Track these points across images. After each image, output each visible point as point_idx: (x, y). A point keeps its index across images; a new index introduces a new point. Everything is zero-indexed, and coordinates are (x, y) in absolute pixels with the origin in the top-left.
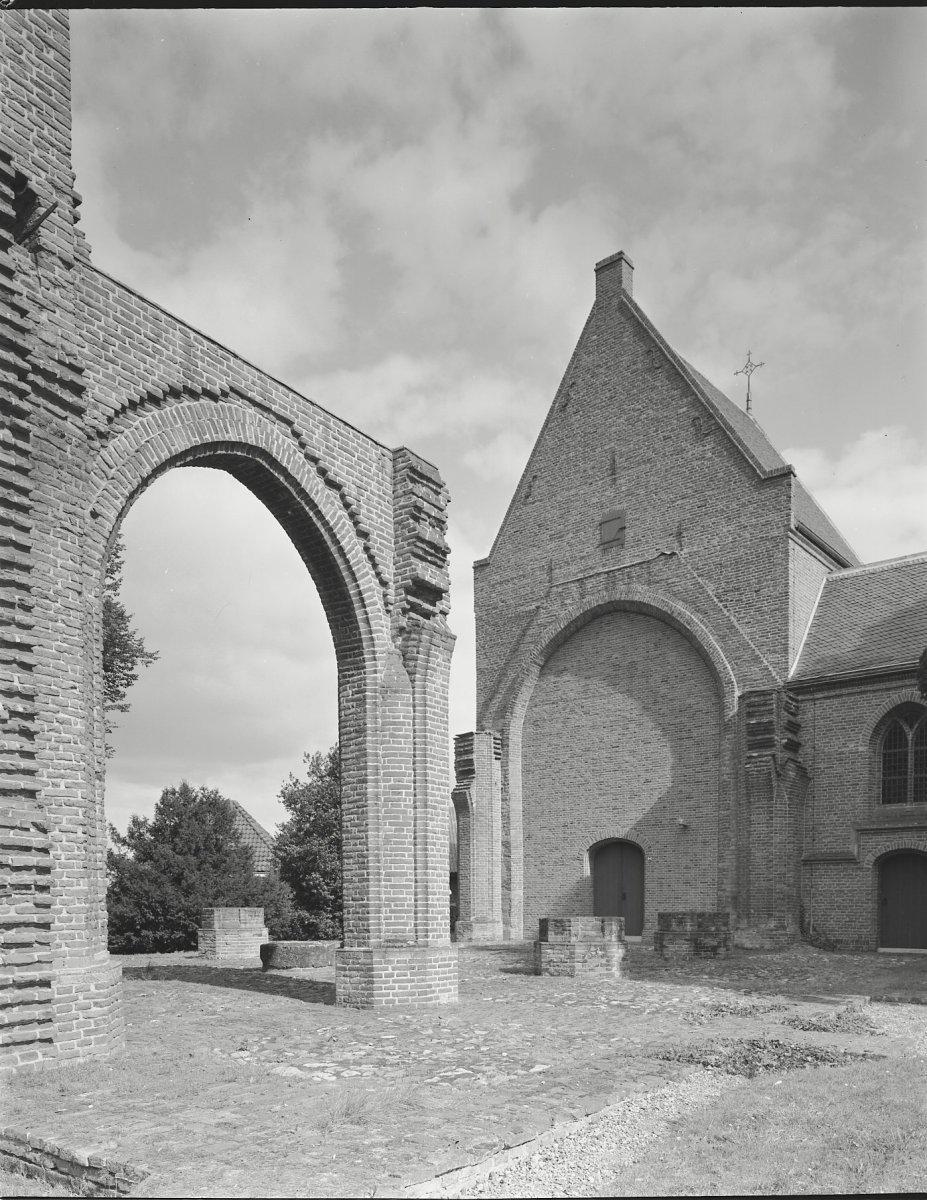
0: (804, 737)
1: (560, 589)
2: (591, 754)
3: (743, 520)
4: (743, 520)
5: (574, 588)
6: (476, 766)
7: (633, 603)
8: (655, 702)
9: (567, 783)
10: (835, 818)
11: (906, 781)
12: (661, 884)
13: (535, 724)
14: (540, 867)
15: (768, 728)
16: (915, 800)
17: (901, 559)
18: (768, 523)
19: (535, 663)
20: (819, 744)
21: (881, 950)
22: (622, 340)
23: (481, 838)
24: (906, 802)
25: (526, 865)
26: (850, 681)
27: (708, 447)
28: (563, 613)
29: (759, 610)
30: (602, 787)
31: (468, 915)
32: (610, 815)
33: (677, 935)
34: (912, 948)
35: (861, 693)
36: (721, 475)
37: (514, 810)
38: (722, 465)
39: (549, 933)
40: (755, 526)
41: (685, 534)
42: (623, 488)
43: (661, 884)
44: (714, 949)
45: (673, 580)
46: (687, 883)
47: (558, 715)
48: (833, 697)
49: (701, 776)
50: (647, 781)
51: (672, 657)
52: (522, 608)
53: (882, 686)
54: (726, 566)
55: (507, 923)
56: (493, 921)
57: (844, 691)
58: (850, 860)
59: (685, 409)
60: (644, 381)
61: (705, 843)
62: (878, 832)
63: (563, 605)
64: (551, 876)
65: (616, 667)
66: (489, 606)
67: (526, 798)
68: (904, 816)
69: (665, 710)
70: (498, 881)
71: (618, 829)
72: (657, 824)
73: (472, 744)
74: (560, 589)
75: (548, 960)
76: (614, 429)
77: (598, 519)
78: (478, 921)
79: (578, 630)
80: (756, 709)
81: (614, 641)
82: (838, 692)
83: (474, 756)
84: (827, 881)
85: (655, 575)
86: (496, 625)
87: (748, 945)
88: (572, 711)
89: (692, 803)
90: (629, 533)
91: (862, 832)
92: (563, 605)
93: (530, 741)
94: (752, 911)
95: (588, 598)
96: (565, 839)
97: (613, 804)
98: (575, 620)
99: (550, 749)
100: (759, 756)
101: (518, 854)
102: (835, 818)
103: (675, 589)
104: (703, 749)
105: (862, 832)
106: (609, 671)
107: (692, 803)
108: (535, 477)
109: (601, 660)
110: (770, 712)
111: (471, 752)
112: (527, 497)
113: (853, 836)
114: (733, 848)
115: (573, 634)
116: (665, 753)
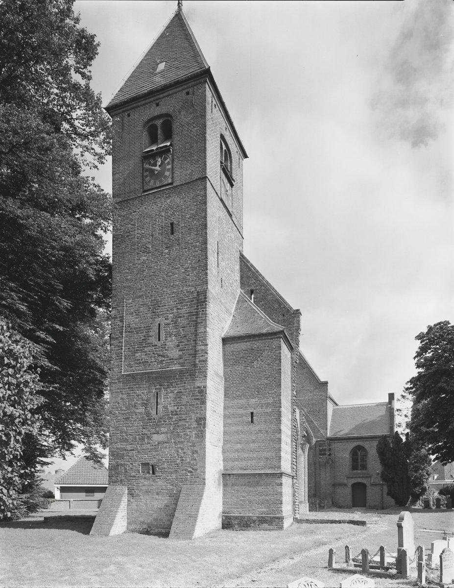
0: (332, 452)
4: (314, 393)
11: (358, 458)
15: (325, 450)
22: (178, 23)
24: (358, 470)
44: (324, 507)
57: (343, 441)
62: (352, 478)
68: (358, 474)
70: (308, 525)
84: (339, 490)
105: (348, 478)
110: (326, 446)
113: (346, 479)
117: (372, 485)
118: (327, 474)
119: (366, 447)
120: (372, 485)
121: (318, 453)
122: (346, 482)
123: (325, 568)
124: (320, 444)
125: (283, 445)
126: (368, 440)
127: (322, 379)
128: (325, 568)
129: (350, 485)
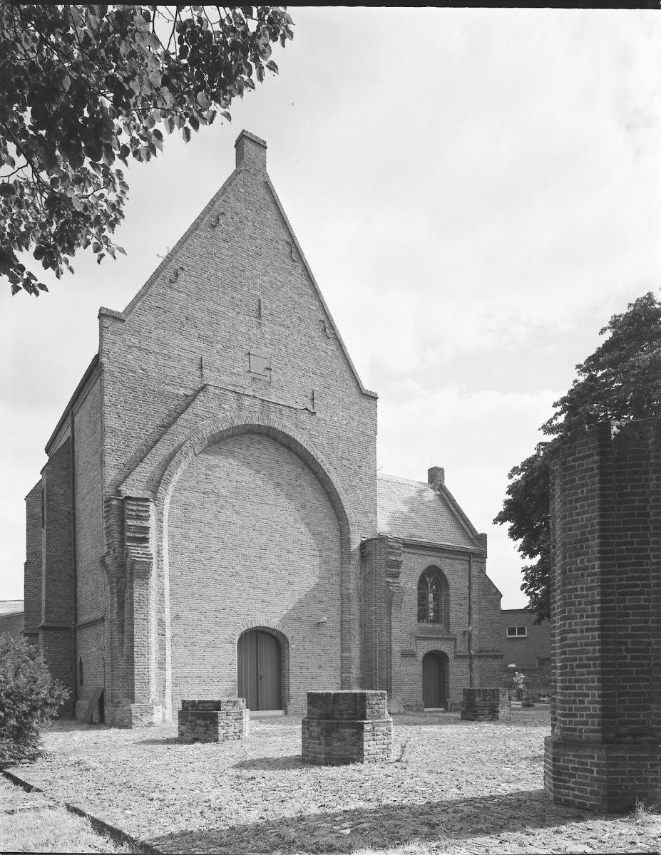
7: (287, 436)
9: (219, 571)
13: (185, 507)
14: (191, 648)
21: (425, 710)
28: (221, 416)
34: (438, 707)
36: (338, 373)
45: (314, 433)
46: (320, 667)
49: (328, 587)
51: (309, 491)
61: (332, 637)
62: (425, 639)
64: (203, 657)
66: (123, 364)
71: (270, 618)
74: (218, 392)
79: (232, 436)
88: (223, 507)
91: (418, 638)
95: (244, 413)
96: (217, 624)
98: (235, 428)
99: (201, 535)
100: (393, 583)
104: (330, 567)
113: (413, 640)
120: (457, 657)
127: (367, 385)
129: (420, 655)
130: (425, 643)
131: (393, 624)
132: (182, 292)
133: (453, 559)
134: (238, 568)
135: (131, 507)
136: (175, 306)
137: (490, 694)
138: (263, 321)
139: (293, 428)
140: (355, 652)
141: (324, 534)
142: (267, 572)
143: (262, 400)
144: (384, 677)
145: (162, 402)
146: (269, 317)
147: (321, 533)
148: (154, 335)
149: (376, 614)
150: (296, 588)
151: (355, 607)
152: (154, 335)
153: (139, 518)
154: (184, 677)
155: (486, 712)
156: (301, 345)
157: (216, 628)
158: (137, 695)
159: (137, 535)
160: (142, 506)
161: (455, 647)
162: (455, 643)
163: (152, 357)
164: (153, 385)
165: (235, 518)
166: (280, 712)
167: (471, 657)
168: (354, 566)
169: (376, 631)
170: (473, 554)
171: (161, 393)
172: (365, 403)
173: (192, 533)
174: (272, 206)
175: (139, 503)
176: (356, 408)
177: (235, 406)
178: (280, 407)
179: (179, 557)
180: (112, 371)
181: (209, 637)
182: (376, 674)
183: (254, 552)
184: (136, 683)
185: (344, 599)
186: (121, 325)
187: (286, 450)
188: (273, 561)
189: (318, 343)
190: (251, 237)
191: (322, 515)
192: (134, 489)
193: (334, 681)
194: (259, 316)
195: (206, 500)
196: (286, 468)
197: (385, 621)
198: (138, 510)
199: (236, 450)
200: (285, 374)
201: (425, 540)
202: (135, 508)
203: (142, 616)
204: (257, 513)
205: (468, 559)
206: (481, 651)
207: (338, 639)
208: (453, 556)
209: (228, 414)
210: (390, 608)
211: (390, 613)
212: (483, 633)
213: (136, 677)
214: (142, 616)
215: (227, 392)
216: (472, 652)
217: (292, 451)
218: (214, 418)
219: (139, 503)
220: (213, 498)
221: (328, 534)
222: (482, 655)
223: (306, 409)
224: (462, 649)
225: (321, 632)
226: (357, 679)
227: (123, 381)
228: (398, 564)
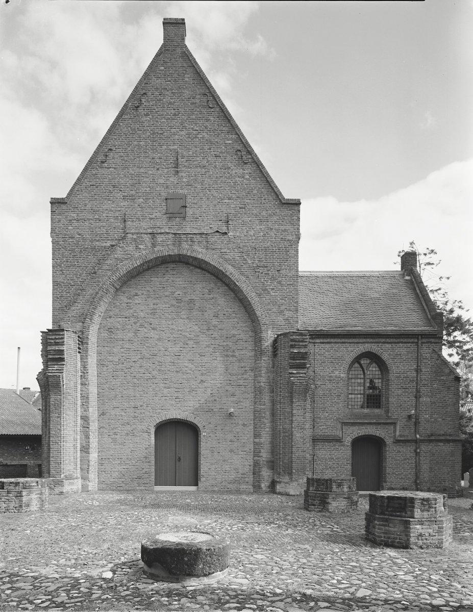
1: (135, 237)
2: (158, 358)
3: (270, 224)
4: (270, 224)
5: (147, 238)
6: (65, 356)
7: (195, 259)
8: (208, 329)
10: (327, 415)
12: (213, 452)
13: (110, 330)
14: (113, 436)
16: (368, 407)
17: (330, 272)
18: (285, 231)
19: (113, 286)
20: (317, 370)
23: (68, 412)
25: (101, 434)
26: (338, 335)
27: (246, 171)
28: (137, 255)
29: (280, 282)
30: (167, 382)
31: (59, 473)
32: (173, 402)
33: (338, 495)
35: (343, 343)
36: (255, 192)
37: (91, 393)
38: (256, 185)
39: (415, 510)
40: (277, 230)
41: (230, 223)
42: (184, 180)
43: (213, 452)
45: (225, 250)
46: (231, 451)
47: (129, 327)
48: (326, 343)
49: (241, 382)
50: (202, 381)
51: (222, 301)
52: (97, 243)
53: (354, 340)
54: (259, 250)
55: (84, 478)
56: (77, 478)
58: (339, 440)
59: (230, 142)
60: (201, 112)
61: (244, 425)
62: (353, 424)
63: (137, 247)
64: (123, 444)
65: (179, 300)
66: (65, 235)
67: (99, 385)
69: (216, 334)
72: (210, 411)
73: (63, 338)
74: (135, 237)
75: (416, 534)
76: (177, 137)
77: (164, 195)
78: (67, 478)
79: (149, 269)
80: (297, 343)
81: (179, 282)
82: (328, 340)
83: (65, 348)
85: (212, 244)
86: (73, 251)
87: (292, 493)
88: (142, 326)
89: (235, 399)
90: (190, 212)
92: (137, 247)
93: (100, 343)
94: (294, 471)
97: (176, 395)
99: (122, 350)
100: (297, 373)
101: (94, 426)
102: (327, 415)
103: (226, 257)
104: (243, 365)
106: (174, 302)
107: (235, 399)
108: (110, 150)
109: (167, 293)
111: (62, 344)
112: (103, 162)
113: (340, 426)
114: (268, 430)
115: (144, 271)
116: (218, 364)
117: (397, 442)
118: (307, 414)
119: (385, 357)
120: (397, 442)
121: (285, 363)
122: (339, 433)
123: (48, 587)
124: (292, 340)
125: (96, 391)
126: (388, 340)
127: (288, 194)
128: (48, 587)
129: (348, 440)
130: (355, 428)
131: (294, 412)
132: (111, 167)
133: (395, 343)
134: (154, 373)
135: (50, 337)
136: (105, 180)
137: (323, 484)
138: (181, 168)
139: (204, 251)
140: (265, 438)
141: (237, 336)
142: (180, 374)
143: (174, 234)
144: (285, 461)
145: (94, 255)
146: (186, 164)
147: (234, 336)
148: (89, 206)
149: (280, 403)
150: (209, 385)
151: (266, 398)
152: (89, 206)
153: (57, 344)
154: (108, 459)
155: (317, 502)
156: (217, 178)
157: (134, 421)
158: (52, 471)
159: (54, 357)
160: (59, 335)
161: (395, 431)
162: (395, 427)
163: (87, 224)
164: (87, 244)
165: (152, 334)
166: (193, 488)
167: (416, 441)
168: (265, 361)
169: (280, 419)
170: (421, 335)
171: (94, 248)
172: (286, 212)
173: (115, 350)
174: (190, 70)
175: (57, 333)
176: (275, 218)
177: (149, 245)
178: (191, 236)
179: (105, 369)
180: (58, 241)
181: (129, 428)
182: (280, 458)
183: (169, 359)
184: (52, 463)
185: (258, 391)
186: (64, 207)
187: (199, 271)
188: (187, 365)
189: (234, 172)
190: (170, 103)
191: (236, 320)
192: (69, 323)
193: (247, 463)
194: (177, 166)
195: (128, 322)
196: (199, 286)
197: (288, 410)
198: (56, 339)
199: (152, 279)
200: (201, 207)
201: (359, 328)
202: (53, 337)
203: (57, 415)
204: (171, 327)
205: (416, 341)
206: (432, 435)
207: (252, 427)
208: (395, 340)
209: (144, 252)
210: (291, 397)
211: (292, 402)
212: (435, 416)
213: (51, 459)
214: (57, 415)
215: (143, 235)
216: (418, 436)
217: (205, 270)
218: (131, 258)
219: (57, 333)
220: (133, 320)
221: (242, 336)
222: (431, 439)
223: (217, 232)
224: (406, 433)
225: (233, 421)
226: (267, 462)
227: (65, 247)
228: (304, 356)
